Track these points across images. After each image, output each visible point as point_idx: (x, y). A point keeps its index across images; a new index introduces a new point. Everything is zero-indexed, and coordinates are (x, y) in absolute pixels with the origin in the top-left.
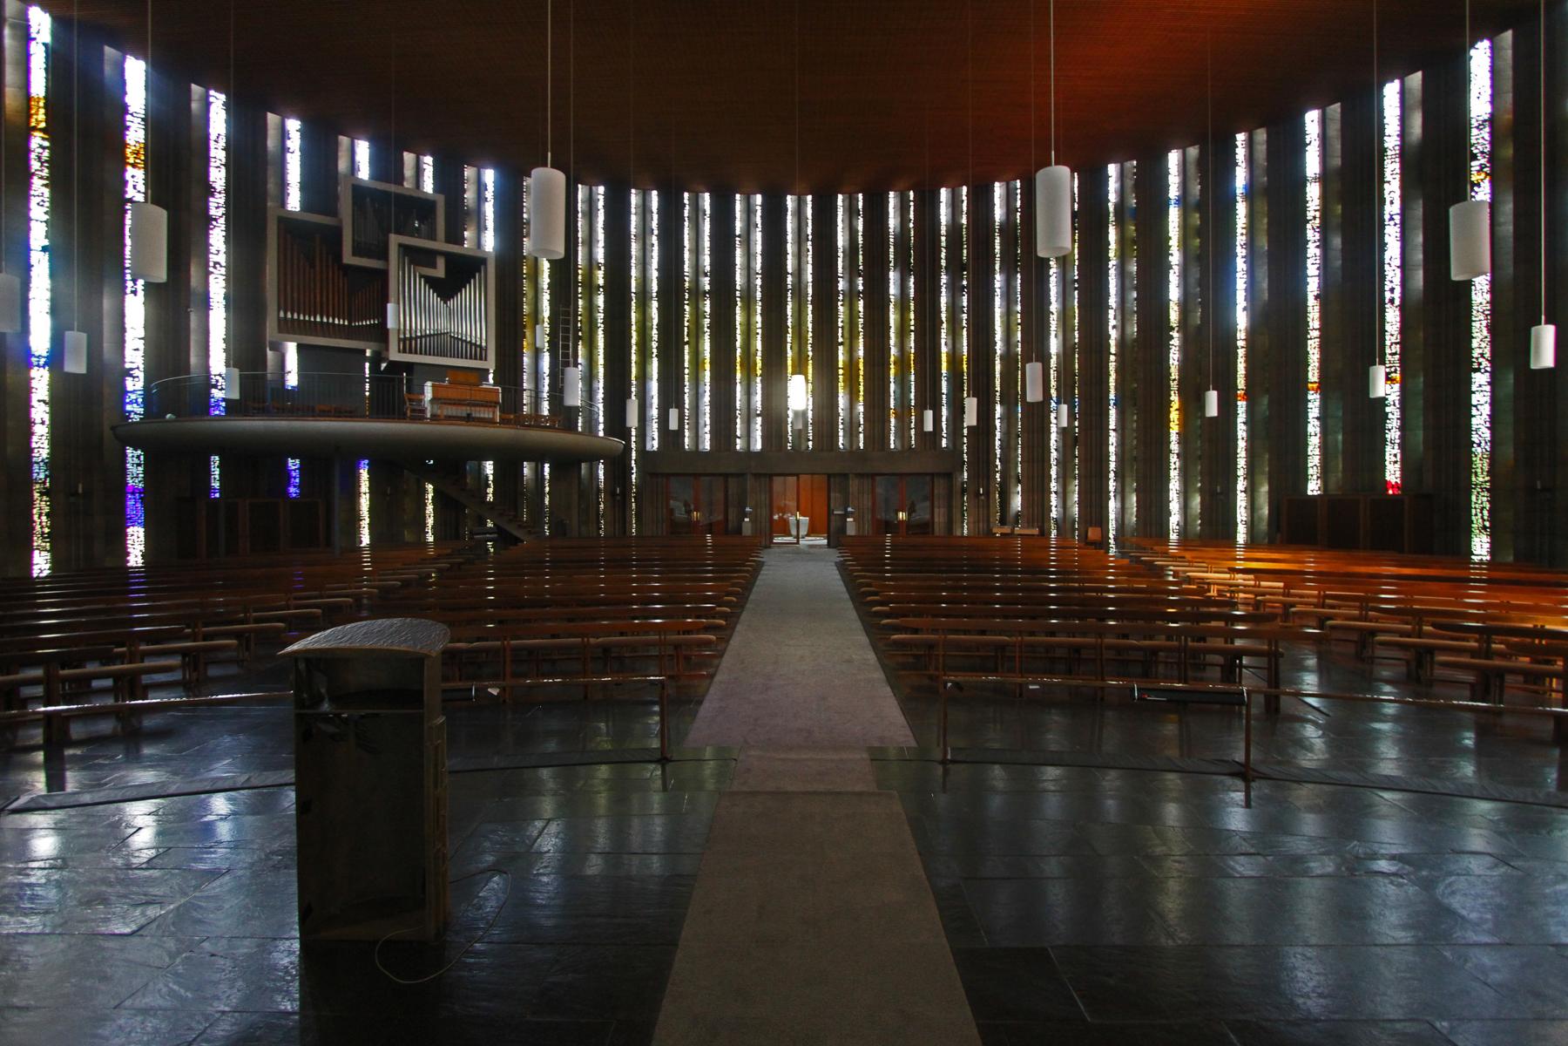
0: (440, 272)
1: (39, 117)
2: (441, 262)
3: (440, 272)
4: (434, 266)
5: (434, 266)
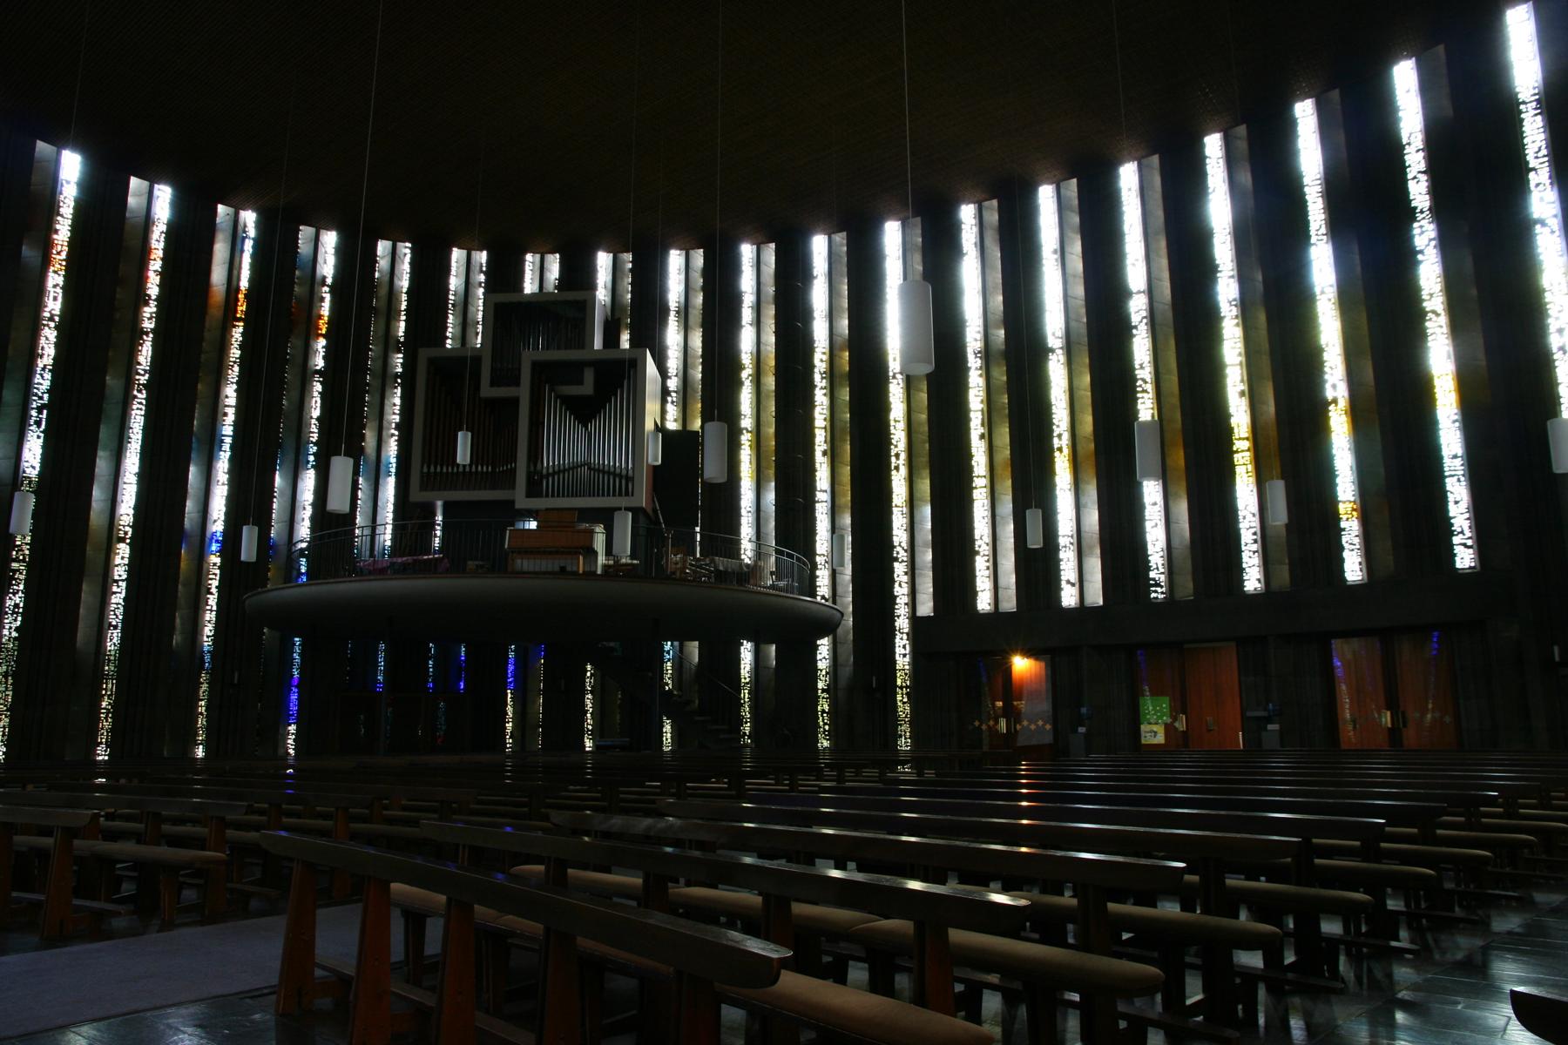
0: (587, 388)
2: (589, 376)
3: (587, 388)
4: (581, 383)
5: (581, 383)
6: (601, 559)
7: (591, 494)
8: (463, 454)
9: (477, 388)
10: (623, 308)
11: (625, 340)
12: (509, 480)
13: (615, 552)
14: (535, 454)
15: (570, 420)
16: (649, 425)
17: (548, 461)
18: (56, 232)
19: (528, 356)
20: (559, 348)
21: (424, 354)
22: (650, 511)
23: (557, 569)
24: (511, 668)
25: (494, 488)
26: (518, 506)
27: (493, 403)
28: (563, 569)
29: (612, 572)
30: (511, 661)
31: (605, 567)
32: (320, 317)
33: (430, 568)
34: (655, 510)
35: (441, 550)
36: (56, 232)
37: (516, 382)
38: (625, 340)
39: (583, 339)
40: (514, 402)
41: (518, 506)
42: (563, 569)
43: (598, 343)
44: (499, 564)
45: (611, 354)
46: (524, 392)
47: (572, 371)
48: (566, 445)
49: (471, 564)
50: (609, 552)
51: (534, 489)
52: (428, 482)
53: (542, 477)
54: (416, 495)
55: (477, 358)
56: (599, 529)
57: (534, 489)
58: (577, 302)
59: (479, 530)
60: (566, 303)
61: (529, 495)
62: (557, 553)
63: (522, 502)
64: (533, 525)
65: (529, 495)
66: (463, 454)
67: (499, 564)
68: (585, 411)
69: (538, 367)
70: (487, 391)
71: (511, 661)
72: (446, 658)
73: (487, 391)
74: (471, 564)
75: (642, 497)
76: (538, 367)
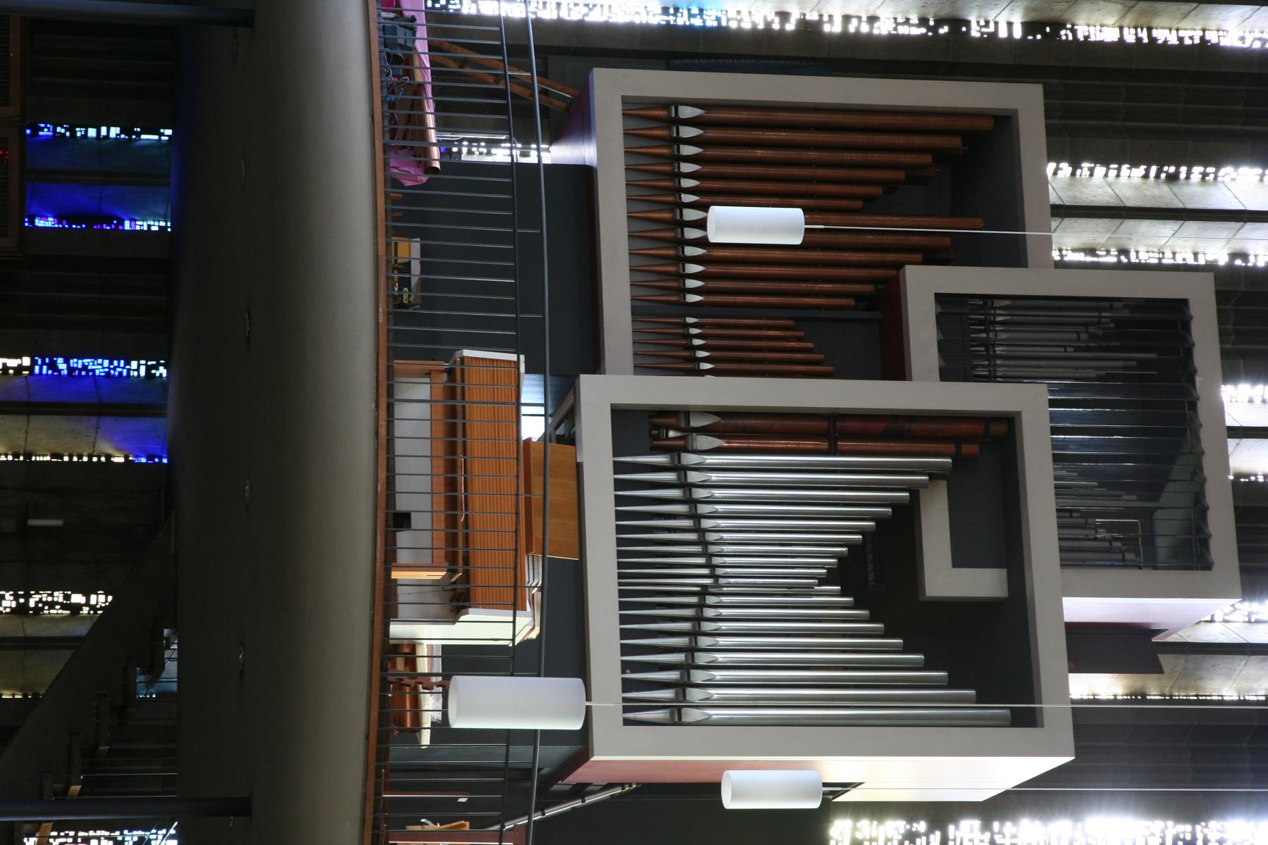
0: (945, 578)
2: (984, 583)
3: (945, 578)
4: (960, 560)
5: (960, 560)
6: (430, 636)
7: (630, 601)
8: (734, 224)
9: (934, 256)
10: (1188, 676)
11: (1103, 686)
12: (664, 353)
13: (461, 683)
14: (739, 428)
15: (853, 529)
16: (836, 768)
17: (718, 470)
18: (1166, 42)
19: (1029, 402)
20: (1060, 491)
21: (1026, 102)
22: (581, 775)
23: (402, 505)
24: (99, 367)
25: (637, 313)
26: (587, 382)
27: (886, 305)
28: (402, 520)
29: (393, 668)
30: (120, 368)
31: (409, 650)
32: (1138, 696)
33: (398, 126)
34: (580, 790)
35: (452, 165)
36: (1166, 42)
37: (955, 367)
38: (1103, 686)
39: (1088, 554)
40: (894, 366)
41: (587, 382)
42: (402, 520)
43: (1083, 608)
44: (417, 330)
45: (1050, 648)
46: (924, 391)
47: (993, 532)
48: (766, 521)
49: (411, 250)
50: (463, 660)
51: (638, 428)
52: (650, 124)
53: (676, 450)
54: (611, 87)
55: (1012, 254)
56: (527, 626)
57: (638, 428)
58: (1205, 542)
59: (506, 272)
60: (1200, 510)
61: (621, 415)
62: (452, 503)
63: (599, 395)
64: (533, 427)
65: (621, 415)
66: (734, 224)
67: (417, 330)
68: (876, 572)
69: (1001, 433)
70: (923, 285)
71: (120, 368)
72: (129, 175)
73: (923, 285)
74: (411, 250)
75: (625, 753)
76: (1001, 433)
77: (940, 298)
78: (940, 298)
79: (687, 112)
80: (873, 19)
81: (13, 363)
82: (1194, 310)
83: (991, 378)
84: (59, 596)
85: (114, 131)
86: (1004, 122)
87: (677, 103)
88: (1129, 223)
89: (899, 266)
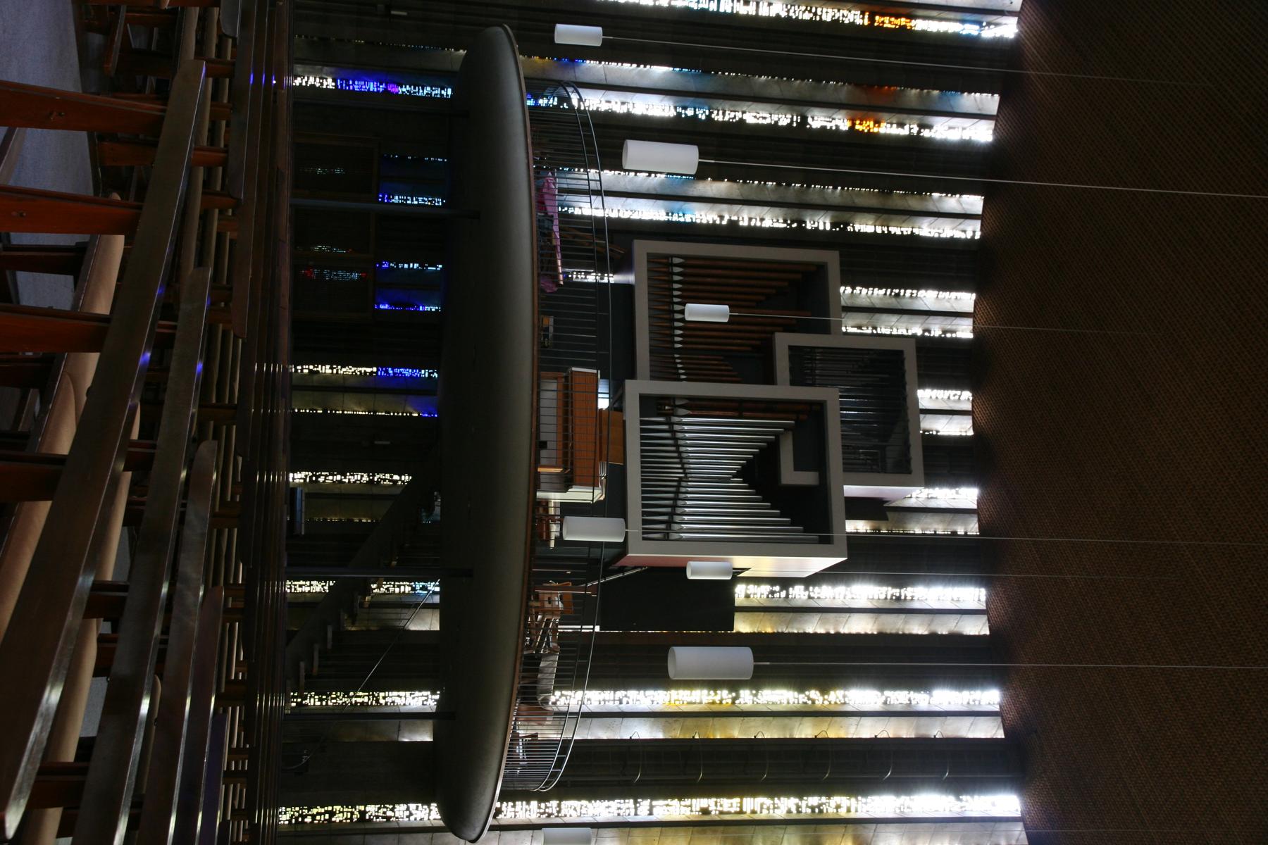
0: (790, 476)
1: (888, 22)
2: (808, 478)
3: (790, 476)
4: (798, 467)
5: (798, 467)
40: (769, 378)
70: (783, 342)
77: (791, 348)
78: (791, 348)
79: (676, 261)
80: (762, 220)
81: (369, 370)
82: (906, 355)
83: (813, 385)
84: (388, 476)
85: (416, 266)
86: (821, 268)
87: (673, 256)
88: (877, 315)
89: (772, 333)
